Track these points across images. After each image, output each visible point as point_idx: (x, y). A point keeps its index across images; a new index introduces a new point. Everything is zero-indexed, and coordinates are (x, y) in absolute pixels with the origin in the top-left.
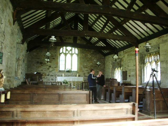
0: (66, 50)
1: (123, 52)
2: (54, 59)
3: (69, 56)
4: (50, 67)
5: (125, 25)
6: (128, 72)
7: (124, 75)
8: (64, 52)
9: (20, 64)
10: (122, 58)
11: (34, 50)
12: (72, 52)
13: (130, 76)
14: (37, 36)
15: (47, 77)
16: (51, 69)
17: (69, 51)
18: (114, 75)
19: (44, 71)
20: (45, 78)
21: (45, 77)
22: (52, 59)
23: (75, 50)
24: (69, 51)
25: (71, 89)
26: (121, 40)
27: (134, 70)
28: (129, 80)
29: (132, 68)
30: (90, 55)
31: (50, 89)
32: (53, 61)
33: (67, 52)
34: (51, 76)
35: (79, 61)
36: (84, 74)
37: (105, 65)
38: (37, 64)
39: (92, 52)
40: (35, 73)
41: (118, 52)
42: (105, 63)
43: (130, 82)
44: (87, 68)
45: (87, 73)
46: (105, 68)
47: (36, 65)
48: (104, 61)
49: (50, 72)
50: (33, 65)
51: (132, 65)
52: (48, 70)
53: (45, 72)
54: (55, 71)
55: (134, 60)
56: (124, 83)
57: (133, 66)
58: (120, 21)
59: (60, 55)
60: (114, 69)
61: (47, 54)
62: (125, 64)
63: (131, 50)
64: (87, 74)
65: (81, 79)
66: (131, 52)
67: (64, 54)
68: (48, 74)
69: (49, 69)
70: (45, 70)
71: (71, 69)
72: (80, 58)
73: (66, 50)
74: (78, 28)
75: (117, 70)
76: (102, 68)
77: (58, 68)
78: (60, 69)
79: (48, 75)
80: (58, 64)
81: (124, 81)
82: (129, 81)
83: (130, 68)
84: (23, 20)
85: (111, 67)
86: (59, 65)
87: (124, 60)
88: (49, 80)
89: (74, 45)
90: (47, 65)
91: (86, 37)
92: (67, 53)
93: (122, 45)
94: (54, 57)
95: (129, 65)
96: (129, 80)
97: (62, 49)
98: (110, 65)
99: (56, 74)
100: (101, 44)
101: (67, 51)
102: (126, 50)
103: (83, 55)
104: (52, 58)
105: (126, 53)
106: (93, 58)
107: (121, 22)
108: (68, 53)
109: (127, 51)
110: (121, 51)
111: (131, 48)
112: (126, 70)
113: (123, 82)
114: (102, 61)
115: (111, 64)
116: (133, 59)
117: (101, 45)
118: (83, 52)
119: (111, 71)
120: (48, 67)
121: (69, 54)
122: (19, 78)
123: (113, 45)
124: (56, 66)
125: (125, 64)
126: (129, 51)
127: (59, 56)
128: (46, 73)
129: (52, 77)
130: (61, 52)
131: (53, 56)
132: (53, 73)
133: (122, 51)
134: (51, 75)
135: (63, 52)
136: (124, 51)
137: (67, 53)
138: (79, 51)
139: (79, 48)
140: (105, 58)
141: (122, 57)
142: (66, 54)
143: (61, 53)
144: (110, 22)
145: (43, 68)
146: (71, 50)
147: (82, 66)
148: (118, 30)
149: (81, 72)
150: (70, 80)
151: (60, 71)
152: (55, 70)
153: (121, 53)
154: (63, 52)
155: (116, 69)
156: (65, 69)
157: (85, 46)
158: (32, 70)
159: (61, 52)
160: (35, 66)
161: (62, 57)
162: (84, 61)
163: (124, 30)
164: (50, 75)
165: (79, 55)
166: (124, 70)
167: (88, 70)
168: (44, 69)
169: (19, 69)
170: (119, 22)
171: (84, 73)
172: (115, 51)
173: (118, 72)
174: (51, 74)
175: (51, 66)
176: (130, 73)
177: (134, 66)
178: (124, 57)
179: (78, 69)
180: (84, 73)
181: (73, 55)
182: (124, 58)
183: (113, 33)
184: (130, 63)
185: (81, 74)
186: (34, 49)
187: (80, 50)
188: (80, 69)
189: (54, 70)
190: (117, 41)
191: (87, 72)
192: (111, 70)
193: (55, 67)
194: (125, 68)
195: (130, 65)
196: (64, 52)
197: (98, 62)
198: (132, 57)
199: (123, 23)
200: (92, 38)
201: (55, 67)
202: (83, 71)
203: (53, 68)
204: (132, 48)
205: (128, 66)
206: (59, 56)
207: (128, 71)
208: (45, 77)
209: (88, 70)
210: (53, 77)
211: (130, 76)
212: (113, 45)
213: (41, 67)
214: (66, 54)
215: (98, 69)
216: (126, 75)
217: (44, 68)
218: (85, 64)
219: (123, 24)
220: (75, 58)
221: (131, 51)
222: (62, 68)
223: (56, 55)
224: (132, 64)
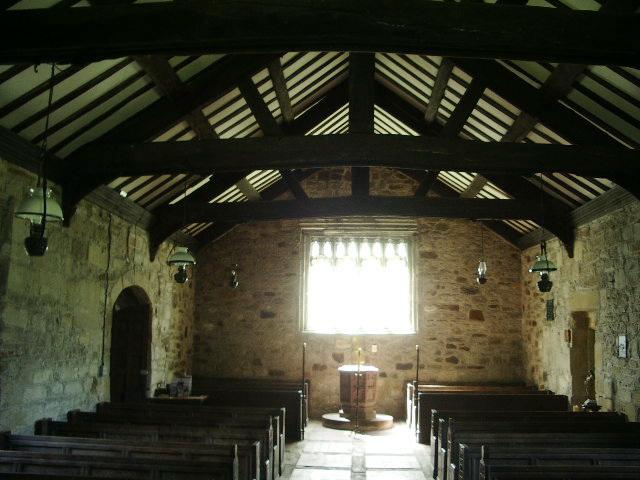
72: (297, 322)
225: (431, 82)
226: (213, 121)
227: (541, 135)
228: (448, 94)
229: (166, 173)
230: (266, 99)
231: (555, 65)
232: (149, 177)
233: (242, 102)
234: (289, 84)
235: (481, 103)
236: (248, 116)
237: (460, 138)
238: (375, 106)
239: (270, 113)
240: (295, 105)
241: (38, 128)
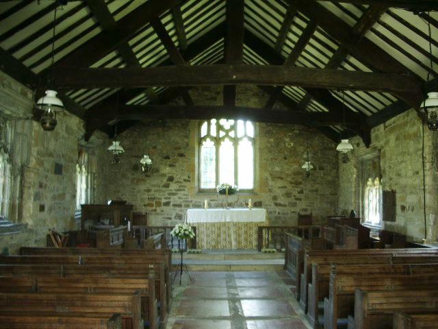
0: (220, 128)
1: (385, 127)
2: (181, 155)
3: (226, 145)
4: (171, 179)
5: (371, 36)
6: (398, 196)
7: (389, 204)
8: (213, 133)
9: (30, 183)
10: (382, 147)
11: (125, 132)
12: (236, 133)
13: (403, 208)
14: (110, 94)
15: (162, 211)
16: (173, 186)
17: (227, 132)
18: (363, 200)
19: (152, 192)
20: (158, 214)
21: (158, 210)
22: (176, 157)
23: (246, 128)
24: (227, 132)
26: (359, 89)
27: (414, 187)
28: (400, 221)
29: (410, 181)
30: (292, 139)
32: (181, 163)
33: (222, 134)
34: (174, 205)
35: (258, 158)
36: (275, 198)
37: (338, 170)
38: (134, 172)
39: (297, 132)
40: (109, 203)
41: (370, 129)
43: (405, 228)
44: (282, 179)
45: (282, 195)
46: (338, 177)
47: (130, 175)
49: (170, 194)
50: (124, 176)
51: (410, 173)
52: (164, 189)
53: (158, 196)
54: (186, 192)
55: (416, 153)
56: (389, 230)
57: (412, 174)
58: (355, 22)
59: (200, 144)
60: (362, 180)
61: (111, 148)
63: (406, 118)
64: (282, 198)
65: (259, 216)
66: (407, 128)
67: (231, 139)
68: (167, 200)
69: (167, 186)
70: (158, 188)
71: (236, 183)
72: (261, 150)
73: (220, 128)
74: (244, 56)
76: (330, 178)
77: (196, 184)
78: (203, 186)
79: (167, 204)
80: (193, 171)
81: (388, 223)
82: (402, 224)
83: (403, 181)
84: (135, 50)
85: (355, 176)
86: (196, 173)
87: (388, 155)
88: (170, 218)
89: (231, 110)
90: (164, 175)
92: (221, 136)
93: (382, 105)
94: (182, 151)
95: (400, 170)
96: (400, 221)
97: (205, 125)
99: (190, 199)
100: (316, 106)
101: (221, 132)
102: (393, 119)
103: (268, 142)
104: (177, 152)
105: (392, 130)
106: (301, 149)
107: (357, 24)
108: (224, 137)
109: (394, 122)
110: (377, 124)
111: (405, 113)
112: (394, 188)
113: (386, 225)
114: (330, 157)
115: (356, 167)
116: (411, 150)
117: (321, 109)
118: (268, 132)
119: (354, 190)
120: (165, 180)
121: (227, 140)
122: (27, 225)
123: (355, 108)
124: (189, 177)
125: (390, 167)
127: (196, 147)
128: (161, 199)
129: (178, 208)
130: (202, 136)
131: (180, 148)
132: (179, 198)
133: (382, 125)
134: (175, 203)
135: (208, 135)
136: (388, 123)
137: (221, 136)
138: (258, 128)
139: (257, 123)
141: (382, 143)
142: (217, 141)
143: (205, 138)
144: (316, 34)
145: (150, 183)
146: (233, 128)
147: (267, 175)
148: (254, 63)
149: (263, 194)
150: (225, 217)
151: (202, 192)
152: (186, 189)
153: (378, 130)
154: (208, 135)
156: (217, 183)
157: (276, 115)
158: (119, 192)
159: (202, 136)
160: (128, 178)
161: (207, 147)
162: (272, 159)
163: (371, 53)
164: (172, 204)
165: (258, 143)
166: (388, 189)
167: (285, 187)
168: (154, 186)
169: (29, 198)
170: (352, 26)
171: (275, 194)
172: (360, 126)
174: (174, 200)
175: (174, 176)
176: (403, 199)
177: (414, 174)
178: (387, 143)
179: (255, 183)
180: (272, 195)
181: (241, 143)
182: (387, 148)
184: (404, 164)
185: (265, 197)
186: (124, 131)
187: (261, 128)
188: (261, 183)
189: (184, 190)
190: (360, 93)
191: (284, 191)
192: (353, 186)
193: (185, 180)
194: (391, 179)
195: (403, 172)
196: (213, 133)
197: (307, 163)
198: (408, 143)
199: (363, 26)
200: (283, 87)
201: (185, 180)
202: (270, 191)
203: (181, 182)
204: (408, 115)
205: (399, 175)
206: (196, 147)
207: (397, 191)
208: (158, 210)
209: (285, 187)
210: (181, 211)
211: (403, 208)
212: (355, 108)
213: (144, 180)
214: (217, 141)
215: (318, 181)
216: (394, 204)
217: (152, 183)
218: (277, 169)
219: (364, 31)
220: (247, 152)
221: (405, 124)
222: (207, 181)
223: (188, 145)
224: (410, 168)
225: (282, 19)
226: (138, 56)
227: (354, 63)
228: (294, 28)
229: (83, 88)
230: (170, 34)
231: (366, 6)
232: (86, 90)
233: (155, 36)
234: (184, 16)
235: (312, 41)
236: (385, 25)
237: (295, 66)
238: (244, 45)
239: (166, 48)
240: (191, 38)
241: (79, 100)
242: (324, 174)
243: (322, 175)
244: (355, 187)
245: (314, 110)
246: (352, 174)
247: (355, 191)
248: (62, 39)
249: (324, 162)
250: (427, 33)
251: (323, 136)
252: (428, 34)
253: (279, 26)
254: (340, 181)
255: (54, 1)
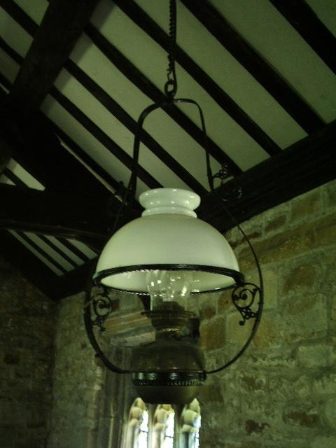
25: (131, 325)
31: (145, 325)
42: (52, 347)
46: (49, 381)
48: (51, 335)
62: (250, 383)
75: (146, 415)
76: (30, 385)
85: (97, 388)
91: (13, 232)
98: (90, 373)
102: (270, 215)
109: (273, 225)
119: (91, 424)
125: (250, 383)
126: (311, 219)
140: (54, 314)
155: (134, 409)
173: (154, 436)
183: (129, 187)
192: (91, 413)
242: (18, 375)
243: (12, 377)
244: (97, 416)
245: (52, 239)
246: (90, 381)
247: (96, 429)
248: (60, 248)
249: (20, 345)
250: (164, 24)
251: (68, 298)
252: (165, 26)
253: (92, 61)
254: (56, 395)
255: (47, 4)
